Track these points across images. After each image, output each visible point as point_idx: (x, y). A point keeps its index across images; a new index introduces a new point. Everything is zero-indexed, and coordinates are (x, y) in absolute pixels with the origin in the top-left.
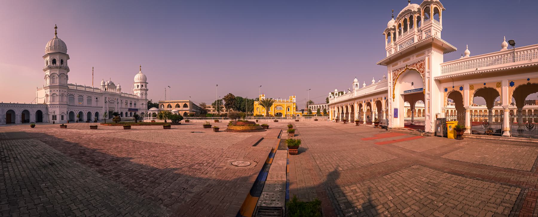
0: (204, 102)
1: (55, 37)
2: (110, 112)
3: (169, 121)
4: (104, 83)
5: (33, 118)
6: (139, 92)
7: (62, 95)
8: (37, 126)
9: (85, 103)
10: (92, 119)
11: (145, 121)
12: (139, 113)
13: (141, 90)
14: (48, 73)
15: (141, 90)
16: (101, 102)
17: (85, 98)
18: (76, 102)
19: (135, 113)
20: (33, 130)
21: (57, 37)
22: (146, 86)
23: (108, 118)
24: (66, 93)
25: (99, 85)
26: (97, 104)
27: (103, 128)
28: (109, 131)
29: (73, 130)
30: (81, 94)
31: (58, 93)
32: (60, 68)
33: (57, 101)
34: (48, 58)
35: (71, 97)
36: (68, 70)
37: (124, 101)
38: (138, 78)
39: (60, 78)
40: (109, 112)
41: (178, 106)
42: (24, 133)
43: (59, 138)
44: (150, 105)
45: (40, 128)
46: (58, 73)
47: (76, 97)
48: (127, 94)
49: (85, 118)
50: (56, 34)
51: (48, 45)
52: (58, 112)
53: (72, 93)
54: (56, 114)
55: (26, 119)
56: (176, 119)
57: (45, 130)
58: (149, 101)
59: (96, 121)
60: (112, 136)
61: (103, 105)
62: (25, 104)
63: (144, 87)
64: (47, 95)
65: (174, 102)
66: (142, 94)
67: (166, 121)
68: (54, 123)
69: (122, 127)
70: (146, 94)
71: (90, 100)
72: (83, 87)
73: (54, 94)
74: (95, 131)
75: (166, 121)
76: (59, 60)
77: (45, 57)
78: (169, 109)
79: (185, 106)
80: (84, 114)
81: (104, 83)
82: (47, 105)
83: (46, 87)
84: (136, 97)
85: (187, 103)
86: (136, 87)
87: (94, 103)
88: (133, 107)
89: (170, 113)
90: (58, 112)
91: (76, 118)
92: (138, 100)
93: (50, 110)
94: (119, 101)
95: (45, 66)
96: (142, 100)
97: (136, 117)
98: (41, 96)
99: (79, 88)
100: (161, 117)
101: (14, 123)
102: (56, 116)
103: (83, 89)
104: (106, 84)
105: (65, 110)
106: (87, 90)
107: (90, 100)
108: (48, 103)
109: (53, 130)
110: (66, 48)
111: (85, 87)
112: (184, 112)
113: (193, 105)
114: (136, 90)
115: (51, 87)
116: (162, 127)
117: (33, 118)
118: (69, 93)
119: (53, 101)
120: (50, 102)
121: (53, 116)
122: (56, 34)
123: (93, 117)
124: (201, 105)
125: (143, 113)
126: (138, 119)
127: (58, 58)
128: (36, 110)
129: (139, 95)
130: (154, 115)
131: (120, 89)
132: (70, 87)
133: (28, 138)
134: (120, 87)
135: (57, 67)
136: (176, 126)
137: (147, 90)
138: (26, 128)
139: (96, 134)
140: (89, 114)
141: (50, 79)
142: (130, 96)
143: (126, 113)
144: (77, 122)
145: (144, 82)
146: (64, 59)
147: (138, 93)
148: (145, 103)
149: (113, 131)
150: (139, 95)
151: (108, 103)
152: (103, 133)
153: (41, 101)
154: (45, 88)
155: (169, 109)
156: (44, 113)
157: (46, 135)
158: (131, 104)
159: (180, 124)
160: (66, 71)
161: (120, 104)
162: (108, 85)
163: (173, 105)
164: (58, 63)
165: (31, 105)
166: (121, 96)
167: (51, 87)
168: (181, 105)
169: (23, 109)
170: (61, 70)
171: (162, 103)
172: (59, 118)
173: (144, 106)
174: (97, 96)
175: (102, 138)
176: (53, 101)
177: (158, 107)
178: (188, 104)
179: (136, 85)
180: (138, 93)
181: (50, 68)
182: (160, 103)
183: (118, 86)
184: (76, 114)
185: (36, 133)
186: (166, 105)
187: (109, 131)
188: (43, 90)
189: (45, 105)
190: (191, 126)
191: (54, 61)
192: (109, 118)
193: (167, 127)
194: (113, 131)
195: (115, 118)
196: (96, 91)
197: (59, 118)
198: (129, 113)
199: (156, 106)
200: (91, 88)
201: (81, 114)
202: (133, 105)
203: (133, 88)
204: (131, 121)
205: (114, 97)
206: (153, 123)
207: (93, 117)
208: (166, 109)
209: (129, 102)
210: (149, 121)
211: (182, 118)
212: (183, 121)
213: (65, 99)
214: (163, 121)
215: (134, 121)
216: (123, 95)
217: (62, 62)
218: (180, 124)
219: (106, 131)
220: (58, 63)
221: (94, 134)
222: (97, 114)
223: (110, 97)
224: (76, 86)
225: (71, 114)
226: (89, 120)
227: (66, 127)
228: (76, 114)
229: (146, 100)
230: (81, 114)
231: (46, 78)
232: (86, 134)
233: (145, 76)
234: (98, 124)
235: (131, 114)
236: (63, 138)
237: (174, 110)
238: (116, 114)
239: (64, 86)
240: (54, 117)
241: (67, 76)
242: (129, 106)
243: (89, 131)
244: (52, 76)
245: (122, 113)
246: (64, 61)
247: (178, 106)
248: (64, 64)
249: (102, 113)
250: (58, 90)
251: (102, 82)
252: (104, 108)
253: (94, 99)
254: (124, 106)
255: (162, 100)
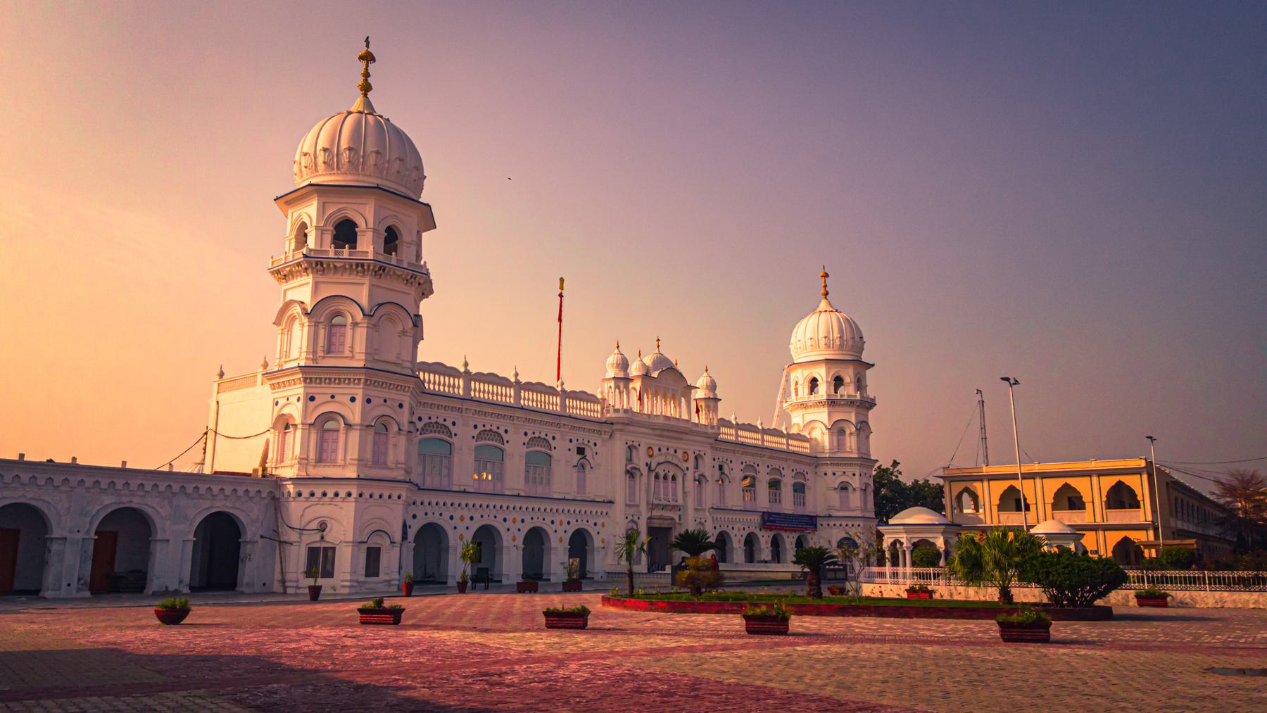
0: (1248, 468)
1: (357, 104)
2: (658, 533)
3: (1028, 594)
4: (624, 365)
5: (172, 560)
6: (822, 415)
7: (378, 428)
8: (201, 612)
9: (515, 478)
10: (552, 570)
11: (868, 590)
12: (826, 538)
13: (831, 403)
14: (303, 290)
15: (831, 403)
16: (607, 475)
17: (516, 447)
18: (465, 472)
19: (799, 544)
20: (177, 639)
21: (368, 104)
22: (860, 384)
23: (642, 566)
24: (404, 417)
25: (594, 374)
26: (582, 485)
27: (620, 622)
28: (658, 641)
29: (443, 635)
30: (492, 423)
31: (355, 413)
32: (380, 270)
33: (347, 459)
34: (310, 211)
35: (433, 437)
36: (422, 284)
37: (735, 471)
38: (810, 335)
39: (373, 328)
40: (651, 531)
41: (1069, 500)
42: (115, 656)
43: (360, 680)
44: (891, 495)
45: (216, 628)
46: (364, 301)
47: (464, 438)
48: (751, 428)
49: (511, 563)
50: (366, 88)
51: (315, 138)
52: (343, 524)
53: (439, 415)
54: (332, 537)
55: (120, 567)
56: (1078, 584)
57: (253, 637)
58: (883, 472)
59: (572, 585)
60: (682, 666)
61: (617, 488)
62: (123, 471)
63: (848, 391)
64: (284, 424)
65: (1044, 475)
66: (837, 430)
67: (1005, 594)
68: (315, 593)
69: (736, 622)
70: (863, 428)
71: (539, 460)
72: (504, 382)
73: (329, 416)
74: (579, 641)
75: (1005, 594)
76: (372, 230)
77: (290, 199)
78: (1013, 519)
79: (1121, 497)
80: (506, 540)
81: (624, 365)
82: (278, 482)
83: (281, 372)
84: (804, 448)
85: (1132, 481)
86: (804, 390)
87: (563, 480)
88: (788, 505)
89: (1029, 543)
90: (343, 524)
91: (457, 567)
92: (814, 460)
93: (299, 512)
94: (708, 468)
95: (287, 251)
96: (835, 461)
97: (814, 560)
98: (246, 427)
99: (480, 391)
100: (974, 570)
101: (33, 593)
102: (329, 553)
103: (507, 395)
104: (634, 370)
105: (393, 516)
106: (530, 400)
107: (539, 460)
108: (288, 472)
109: (323, 636)
110: (419, 167)
111: (519, 386)
112: (1115, 537)
113: (1176, 497)
114: (804, 406)
115: (310, 374)
116: (991, 628)
117: (172, 560)
118: (425, 413)
119: (320, 460)
120: (303, 461)
121: (313, 552)
122: (366, 88)
123: (558, 562)
124: (1229, 490)
125: (848, 544)
126: (825, 581)
127: (365, 215)
128: (198, 511)
129: (821, 435)
130: (925, 555)
131: (713, 401)
132: (432, 381)
133: (151, 689)
134: (712, 386)
135: (359, 267)
136: (1084, 629)
137: (868, 404)
138: (131, 628)
139: (584, 655)
140: (536, 540)
141: (315, 326)
142: (771, 442)
143: (750, 541)
144: (462, 588)
145: (850, 360)
146: (406, 221)
147: (812, 423)
148: (856, 483)
149: (686, 642)
150: (821, 435)
151: (643, 480)
152: (627, 654)
153: (238, 457)
154: (274, 377)
155: (1013, 519)
156: (251, 532)
157: (265, 668)
158: (775, 485)
159: (1106, 614)
160: (412, 291)
161: (710, 489)
162: (646, 376)
163: (1040, 493)
164: (367, 246)
165: (171, 475)
166: (716, 442)
167: (310, 374)
168: (1093, 491)
169: (110, 502)
170: (386, 282)
171: (966, 482)
172: (346, 564)
173: (855, 499)
174: (582, 437)
175: (621, 679)
176: (320, 460)
177: (938, 508)
178: (1140, 485)
179: (800, 376)
180: (812, 423)
181: (315, 264)
182: (951, 479)
183: (702, 382)
184: (459, 538)
185: (202, 659)
186: (991, 493)
187: (658, 641)
188: (262, 393)
189: (264, 487)
190: (1194, 628)
191: (345, 233)
192: (651, 570)
193: (1025, 629)
194: (686, 642)
195: (684, 566)
196: (578, 408)
197: (346, 564)
198: (764, 539)
199: (927, 496)
200: (550, 391)
201: (486, 538)
202: (787, 492)
203: (786, 393)
204: (786, 590)
205: (681, 446)
206: (918, 605)
207: (558, 562)
208: (990, 515)
209: (764, 478)
210: (891, 586)
211: (1118, 580)
212: (1121, 598)
213: (398, 450)
214: (990, 594)
215: (803, 590)
216: (727, 434)
217: (391, 239)
218: (1106, 614)
219: (640, 643)
220: (367, 246)
221: (572, 657)
222: (580, 543)
223: (655, 443)
224: (468, 376)
225: (430, 539)
226: (532, 581)
227: (394, 617)
228: (459, 538)
229: (865, 460)
230: (486, 538)
231: (283, 316)
232: (527, 658)
233: (853, 326)
234: (591, 601)
235: (776, 544)
236: (383, 680)
237: (1046, 525)
238: (693, 542)
239: (394, 374)
240: (320, 560)
241: (417, 321)
242: (763, 501)
243: (544, 642)
244: (325, 316)
245: (723, 541)
246: (406, 236)
247: (1069, 500)
248: (406, 254)
249: (609, 535)
250: (359, 393)
251: (613, 359)
252: (619, 509)
253: (563, 453)
254: (734, 497)
255: (964, 462)
